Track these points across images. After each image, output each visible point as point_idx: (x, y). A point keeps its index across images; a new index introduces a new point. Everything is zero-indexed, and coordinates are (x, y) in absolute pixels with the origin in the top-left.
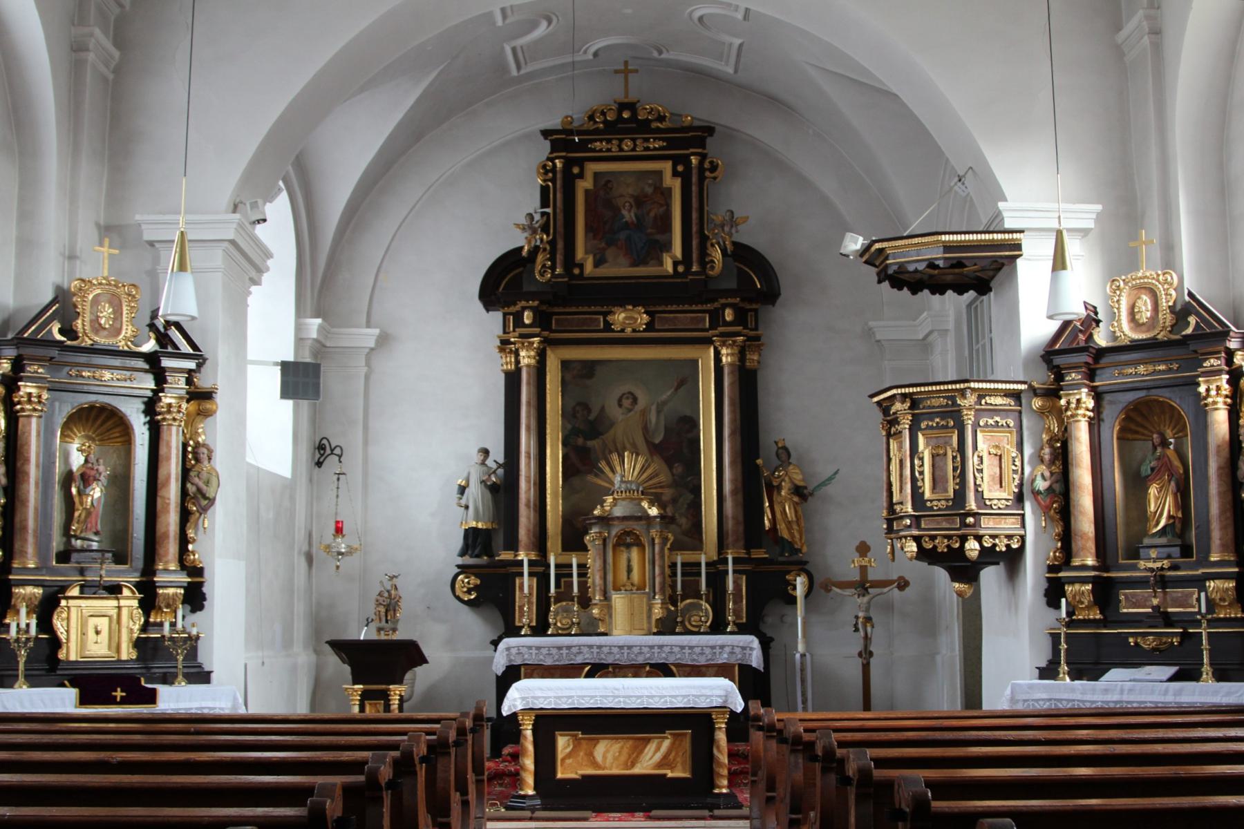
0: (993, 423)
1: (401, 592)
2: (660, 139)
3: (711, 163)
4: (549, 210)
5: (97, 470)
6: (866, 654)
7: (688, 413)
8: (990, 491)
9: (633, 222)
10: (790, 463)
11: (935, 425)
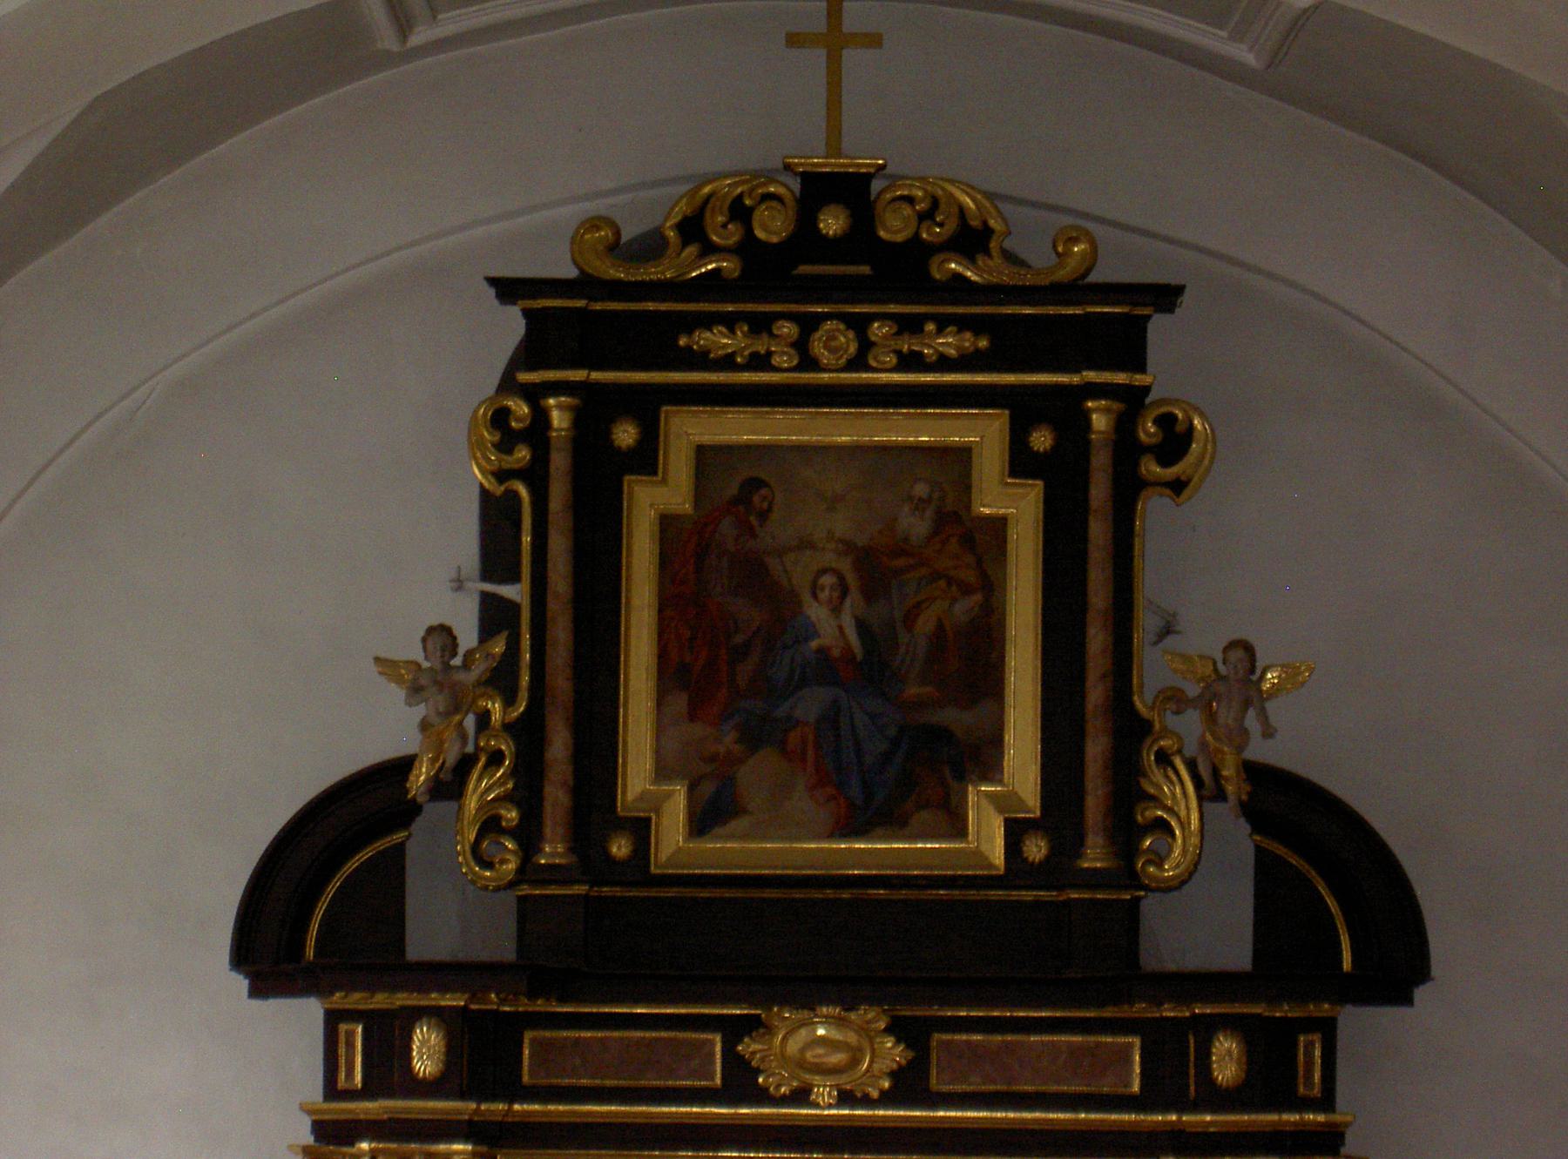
3: (1166, 421)
4: (508, 591)
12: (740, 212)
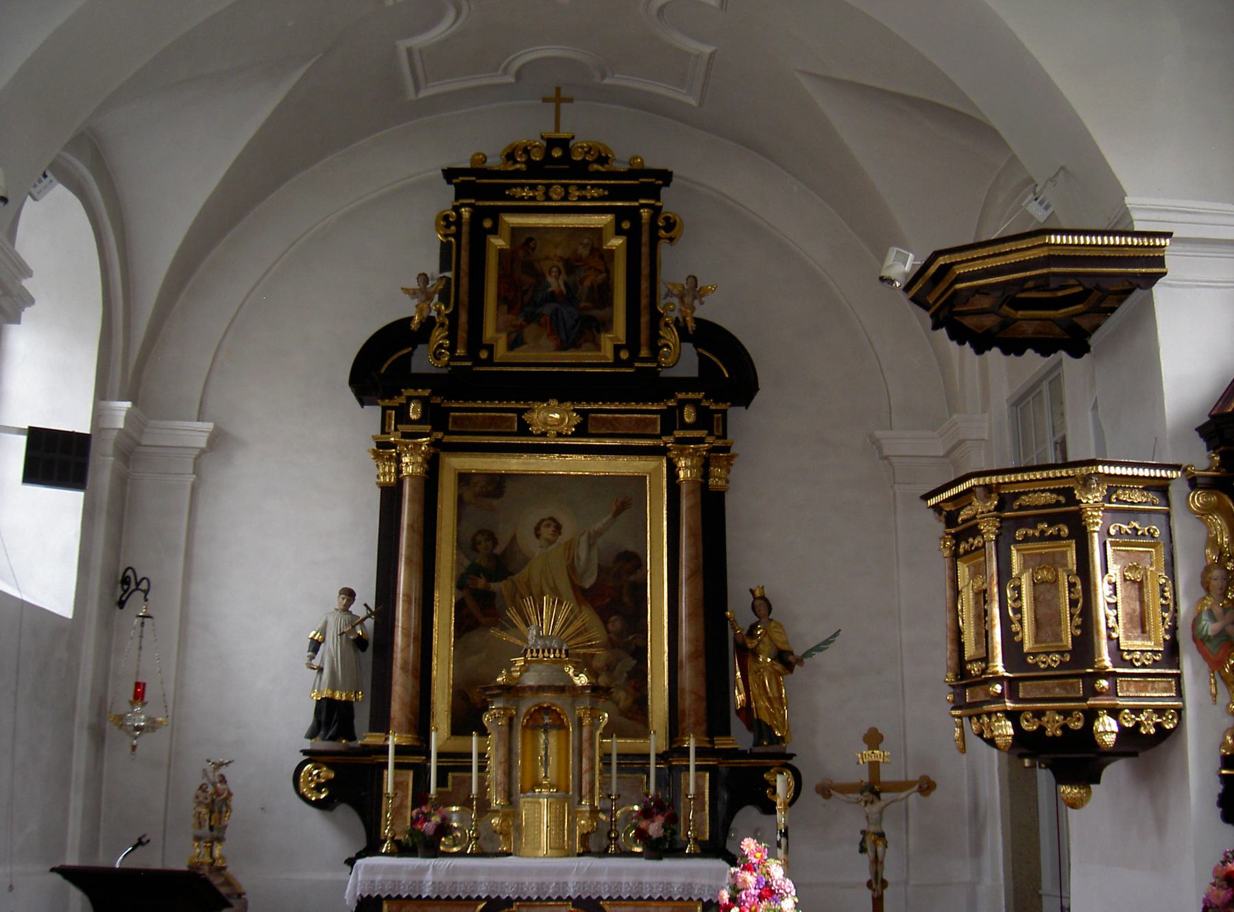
1: (232, 785)
2: (599, 186)
3: (667, 219)
4: (448, 274)
6: (877, 883)
7: (631, 547)
8: (1128, 638)
11: (1037, 534)
12: (526, 151)
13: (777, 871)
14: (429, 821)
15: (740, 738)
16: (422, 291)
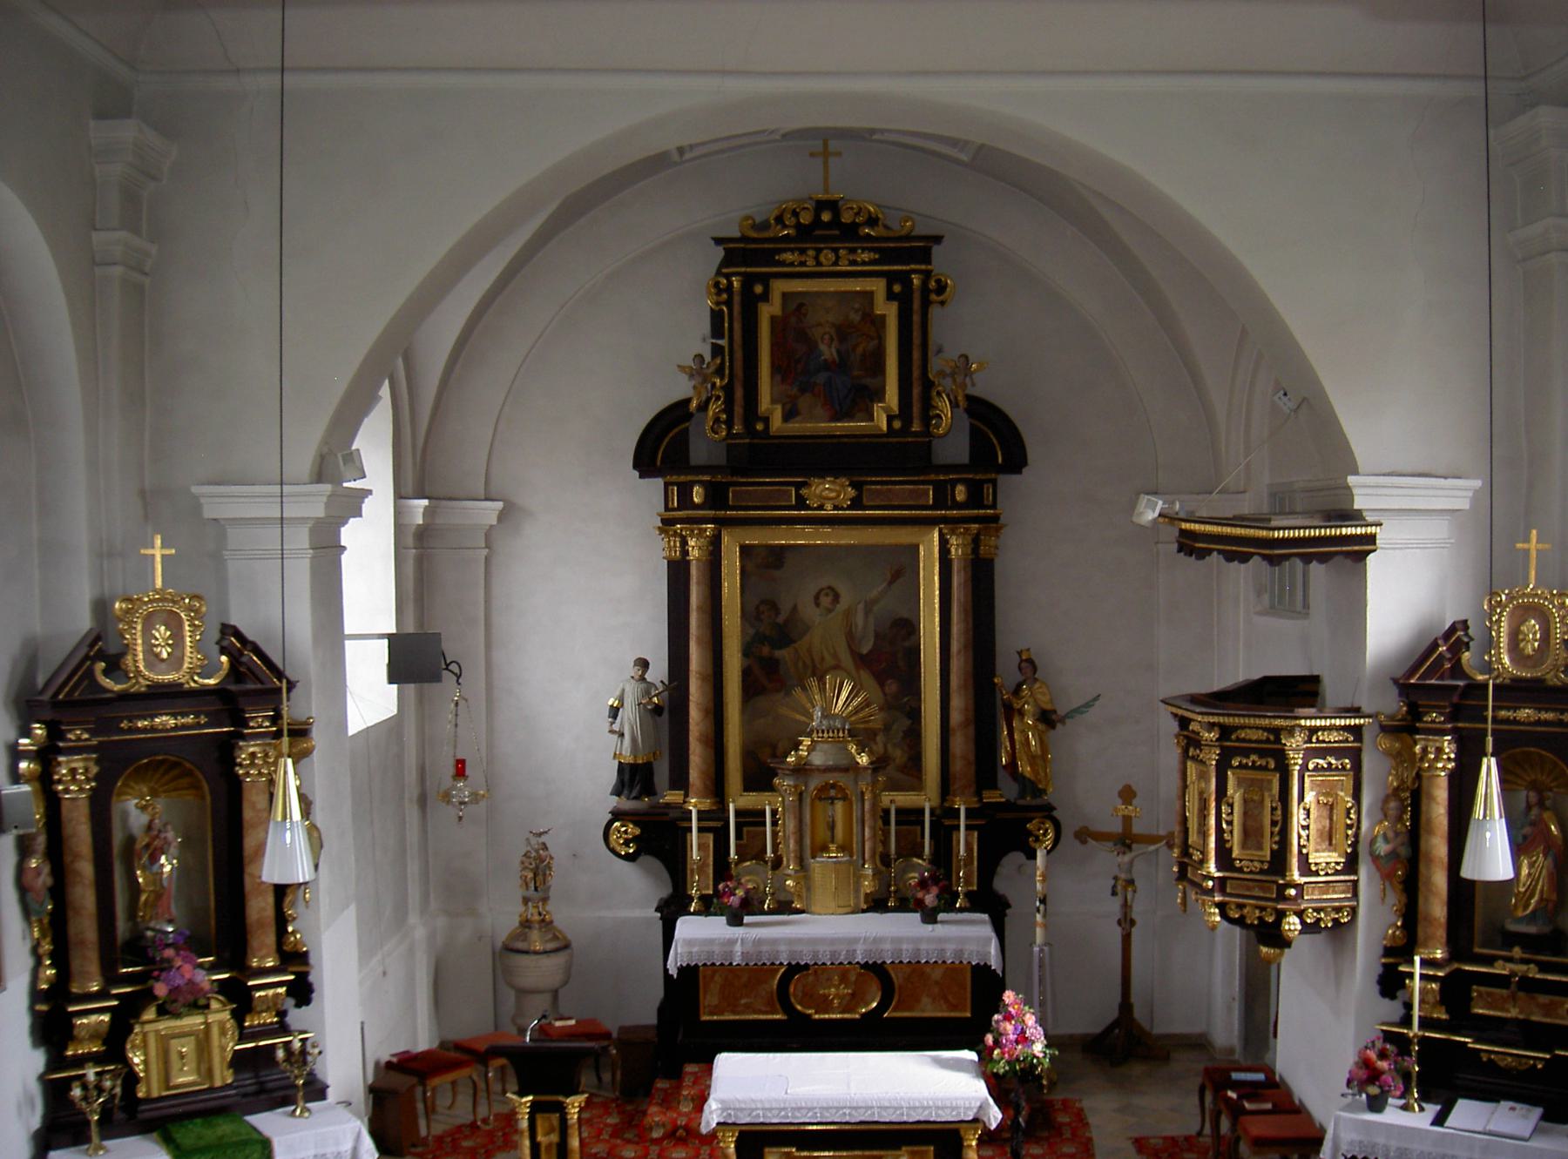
0: (1325, 766)
1: (552, 850)
3: (938, 281)
4: (723, 342)
5: (165, 838)
7: (905, 614)
9: (834, 362)
10: (1036, 680)
13: (1030, 1020)
14: (735, 895)
15: (1006, 791)
16: (697, 371)
